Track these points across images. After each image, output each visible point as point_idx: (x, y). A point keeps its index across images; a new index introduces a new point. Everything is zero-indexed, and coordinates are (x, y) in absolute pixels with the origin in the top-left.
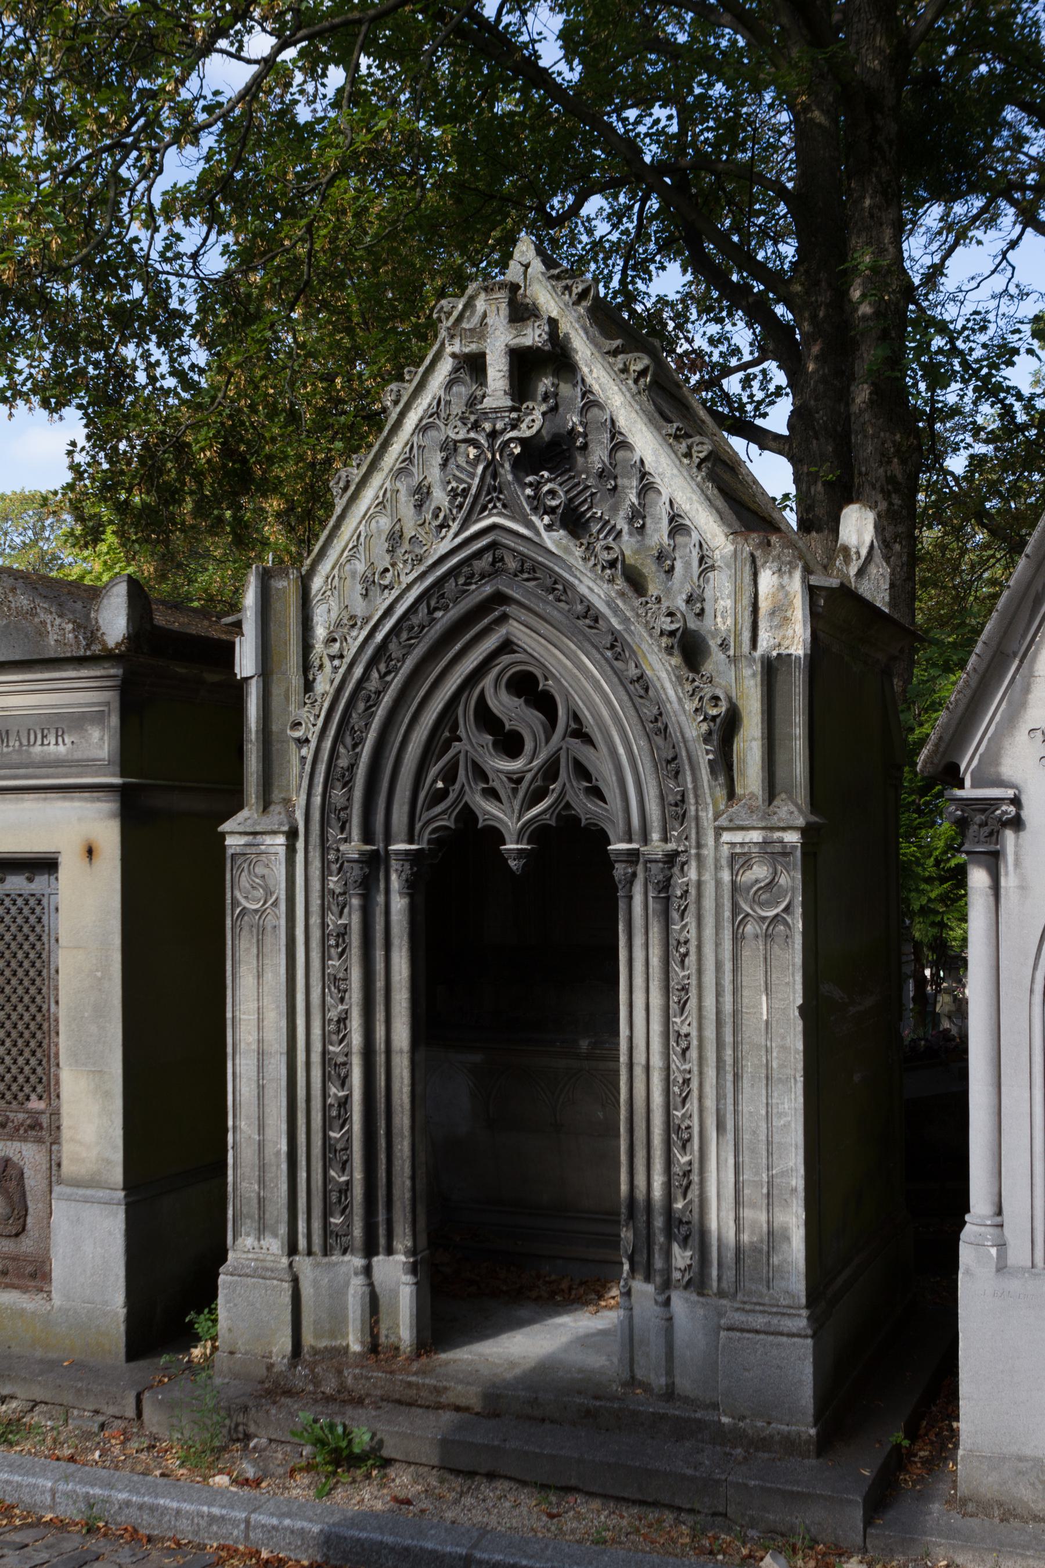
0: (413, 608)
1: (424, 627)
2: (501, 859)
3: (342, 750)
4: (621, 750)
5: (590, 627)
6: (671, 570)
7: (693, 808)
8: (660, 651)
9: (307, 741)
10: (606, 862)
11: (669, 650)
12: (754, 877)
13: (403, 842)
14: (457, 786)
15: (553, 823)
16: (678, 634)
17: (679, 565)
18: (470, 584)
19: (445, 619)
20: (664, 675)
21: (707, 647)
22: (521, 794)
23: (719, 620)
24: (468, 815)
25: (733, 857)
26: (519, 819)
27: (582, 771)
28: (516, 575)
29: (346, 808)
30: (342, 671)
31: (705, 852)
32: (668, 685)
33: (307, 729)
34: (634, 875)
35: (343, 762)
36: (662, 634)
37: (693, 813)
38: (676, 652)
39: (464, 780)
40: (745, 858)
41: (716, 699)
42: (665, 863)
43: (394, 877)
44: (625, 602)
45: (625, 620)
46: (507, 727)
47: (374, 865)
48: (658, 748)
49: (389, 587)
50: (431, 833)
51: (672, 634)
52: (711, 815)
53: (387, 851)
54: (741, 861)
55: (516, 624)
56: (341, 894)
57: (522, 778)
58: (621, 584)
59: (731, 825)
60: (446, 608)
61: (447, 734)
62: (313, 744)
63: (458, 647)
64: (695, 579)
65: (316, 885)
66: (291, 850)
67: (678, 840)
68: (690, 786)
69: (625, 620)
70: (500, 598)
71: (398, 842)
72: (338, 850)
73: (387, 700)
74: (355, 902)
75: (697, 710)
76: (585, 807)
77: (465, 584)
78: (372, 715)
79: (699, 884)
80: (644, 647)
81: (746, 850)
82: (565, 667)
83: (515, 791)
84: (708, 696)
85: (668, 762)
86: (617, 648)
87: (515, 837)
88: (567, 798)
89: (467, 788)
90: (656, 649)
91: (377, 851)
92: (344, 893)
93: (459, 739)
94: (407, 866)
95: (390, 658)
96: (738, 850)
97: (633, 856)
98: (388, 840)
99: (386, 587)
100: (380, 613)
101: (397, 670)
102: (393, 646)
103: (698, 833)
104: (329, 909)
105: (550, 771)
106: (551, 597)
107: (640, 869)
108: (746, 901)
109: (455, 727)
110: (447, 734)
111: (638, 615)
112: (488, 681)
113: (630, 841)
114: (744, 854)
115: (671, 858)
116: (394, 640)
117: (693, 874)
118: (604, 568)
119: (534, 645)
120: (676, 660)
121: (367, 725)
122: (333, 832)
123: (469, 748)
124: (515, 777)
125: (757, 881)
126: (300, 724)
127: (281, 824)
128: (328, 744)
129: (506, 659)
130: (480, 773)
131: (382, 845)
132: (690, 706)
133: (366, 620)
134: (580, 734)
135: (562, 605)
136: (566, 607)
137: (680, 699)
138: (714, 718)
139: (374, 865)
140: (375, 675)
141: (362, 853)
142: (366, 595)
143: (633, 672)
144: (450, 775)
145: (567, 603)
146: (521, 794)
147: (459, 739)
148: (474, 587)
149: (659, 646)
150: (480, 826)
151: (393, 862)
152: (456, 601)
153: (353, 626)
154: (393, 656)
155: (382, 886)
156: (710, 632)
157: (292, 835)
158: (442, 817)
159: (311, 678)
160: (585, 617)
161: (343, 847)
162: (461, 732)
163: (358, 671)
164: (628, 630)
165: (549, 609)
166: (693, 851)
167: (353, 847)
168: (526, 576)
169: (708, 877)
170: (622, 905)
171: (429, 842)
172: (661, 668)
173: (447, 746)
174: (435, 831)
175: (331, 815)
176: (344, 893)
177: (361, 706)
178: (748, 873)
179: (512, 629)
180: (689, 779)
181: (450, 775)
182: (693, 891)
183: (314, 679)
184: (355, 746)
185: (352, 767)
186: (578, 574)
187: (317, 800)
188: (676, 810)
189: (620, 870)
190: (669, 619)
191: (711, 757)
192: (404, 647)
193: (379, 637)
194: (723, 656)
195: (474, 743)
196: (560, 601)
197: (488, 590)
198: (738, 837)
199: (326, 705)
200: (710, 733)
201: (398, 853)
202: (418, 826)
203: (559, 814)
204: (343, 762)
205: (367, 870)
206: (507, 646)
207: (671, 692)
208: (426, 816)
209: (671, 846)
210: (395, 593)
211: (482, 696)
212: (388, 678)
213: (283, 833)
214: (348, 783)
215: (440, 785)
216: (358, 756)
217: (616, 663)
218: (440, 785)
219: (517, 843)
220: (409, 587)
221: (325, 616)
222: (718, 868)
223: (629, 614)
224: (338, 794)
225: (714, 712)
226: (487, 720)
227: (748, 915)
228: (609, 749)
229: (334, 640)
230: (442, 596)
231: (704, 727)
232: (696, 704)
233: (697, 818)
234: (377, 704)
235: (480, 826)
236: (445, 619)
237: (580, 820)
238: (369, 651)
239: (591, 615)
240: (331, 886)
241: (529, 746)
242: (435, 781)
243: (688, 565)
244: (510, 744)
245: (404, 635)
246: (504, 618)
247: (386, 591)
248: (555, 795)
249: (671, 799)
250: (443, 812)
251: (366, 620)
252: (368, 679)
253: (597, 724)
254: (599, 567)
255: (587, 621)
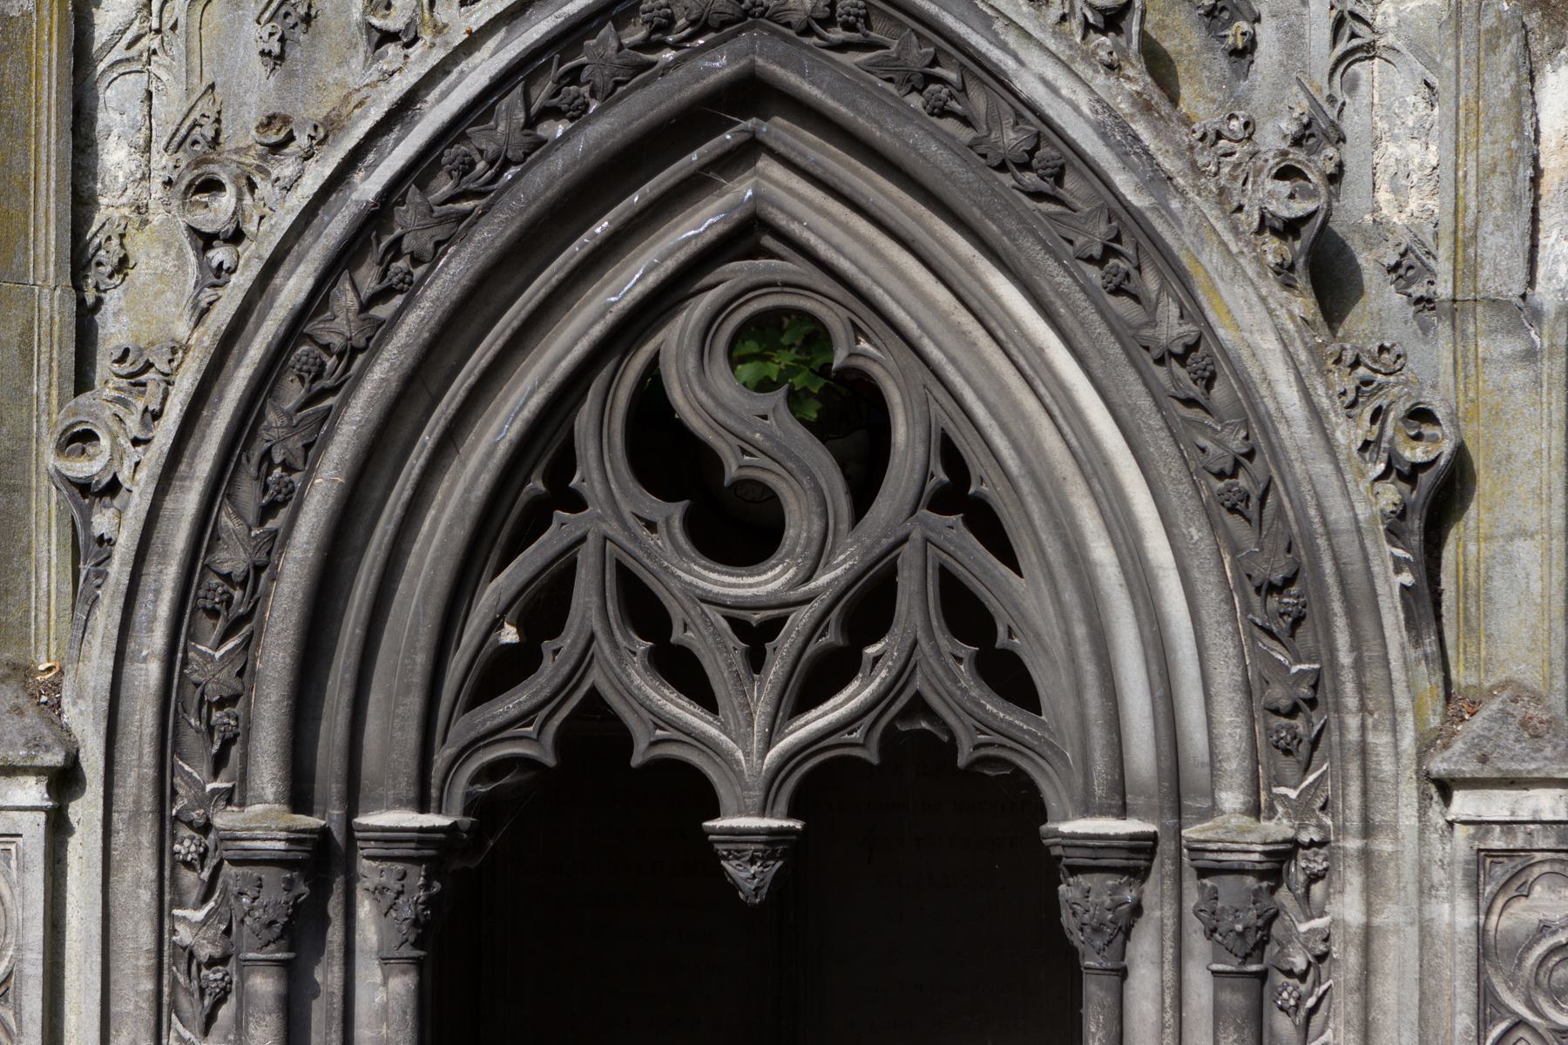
0: (479, 108)
1: (507, 164)
2: (704, 857)
3: (228, 521)
4: (1102, 552)
5: (1038, 196)
6: (1244, 53)
7: (1353, 722)
8: (1262, 275)
9: (113, 487)
10: (1045, 867)
11: (1284, 272)
12: (1534, 918)
13: (399, 803)
14: (569, 640)
15: (871, 755)
16: (1309, 232)
17: (1266, 33)
18: (661, 46)
19: (574, 146)
20: (1269, 344)
21: (1356, 270)
22: (776, 668)
23: (1383, 196)
24: (595, 729)
25: (1483, 858)
26: (769, 745)
27: (965, 612)
28: (807, 31)
29: (232, 700)
30: (241, 282)
31: (1383, 845)
32: (1280, 374)
33: (117, 454)
34: (1137, 910)
35: (232, 559)
36: (1265, 224)
37: (1353, 736)
38: (1302, 280)
39: (918, 618)
40: (1510, 865)
41: (1421, 415)
42: (1261, 875)
43: (365, 909)
44: (1158, 134)
45: (1158, 181)
46: (732, 471)
47: (321, 864)
48: (1235, 550)
49: (407, 38)
50: (476, 779)
51: (1290, 229)
52: (1408, 742)
53: (350, 829)
54: (1500, 872)
55: (777, 171)
56: (212, 963)
57: (779, 623)
58: (1137, 79)
59: (1487, 772)
60: (578, 114)
61: (537, 485)
62: (138, 500)
63: (601, 227)
64: (1321, 78)
65: (137, 934)
66: (58, 827)
67: (1300, 810)
68: (1345, 658)
69: (1158, 181)
70: (751, 93)
71: (379, 805)
72: (206, 828)
73: (382, 373)
74: (264, 985)
75: (1366, 445)
76: (969, 709)
77: (649, 45)
78: (328, 419)
79: (1368, 934)
80: (1211, 259)
81: (1519, 843)
82: (930, 303)
83: (756, 661)
84: (1401, 408)
85: (1273, 589)
86: (1125, 255)
87: (757, 795)
88: (918, 683)
89: (602, 642)
90: (1251, 270)
91: (325, 832)
92: (223, 960)
93: (576, 503)
94: (417, 876)
95: (395, 249)
96: (1496, 841)
97: (1136, 858)
98: (352, 803)
99: (388, 37)
100: (376, 114)
101: (410, 289)
102: (406, 216)
103: (1365, 792)
104: (174, 1007)
105: (869, 606)
106: (915, 101)
107: (1155, 892)
108: (1512, 981)
109: (566, 462)
110: (537, 485)
111: (1196, 170)
112: (675, 336)
113: (1123, 812)
114: (1510, 853)
115: (1281, 857)
116: (413, 194)
117: (1349, 908)
118: (1087, 26)
119: (839, 236)
120: (1303, 304)
121: (312, 449)
122: (193, 771)
123: (612, 528)
124: (756, 617)
125: (1544, 929)
126: (89, 436)
127: (36, 744)
128: (187, 502)
129: (737, 273)
130: (642, 608)
131: (336, 812)
132: (1349, 433)
133: (327, 131)
134: (956, 492)
135: (949, 124)
136: (966, 135)
137: (1316, 415)
138: (1411, 474)
139: (321, 864)
140: (346, 298)
141: (296, 839)
142: (281, 57)
143: (1171, 328)
144: (544, 608)
145: (966, 121)
146: (776, 668)
147: (576, 503)
148: (669, 55)
149: (1259, 260)
150: (637, 760)
151: (364, 865)
152: (610, 95)
153: (276, 148)
154: (408, 244)
155: (335, 935)
156: (1358, 228)
157: (65, 781)
158: (519, 726)
159: (90, 298)
160: (1025, 166)
161: (224, 819)
162: (586, 478)
163: (294, 287)
164: (1162, 207)
165: (915, 135)
166: (1353, 844)
167: (263, 819)
168: (837, 34)
169: (1389, 915)
170: (1095, 993)
171: (472, 805)
172: (1257, 320)
173: (534, 523)
174: (492, 771)
175: (194, 718)
176: (223, 960)
177: (293, 392)
178: (1518, 906)
179: (767, 187)
180: (1342, 639)
181: (544, 608)
182: (1348, 958)
183: (99, 302)
184: (268, 511)
185: (260, 571)
186: (1011, 39)
187: (147, 673)
188: (1295, 725)
189: (1082, 898)
190: (1285, 187)
191: (1407, 578)
192: (443, 220)
193: (368, 186)
194: (1398, 299)
195: (617, 514)
196: (944, 113)
197: (720, 66)
198: (1497, 805)
199: (186, 383)
200: (1402, 514)
201: (390, 837)
202: (441, 757)
203: (890, 727)
204: (232, 559)
205: (303, 889)
206: (748, 235)
207: (1289, 394)
208: (466, 726)
209: (1279, 828)
210: (422, 59)
211: (652, 376)
212: (382, 311)
213: (38, 771)
214: (243, 624)
215: (510, 635)
216: (276, 542)
217: (1112, 301)
218: (510, 635)
219: (762, 813)
220: (474, 40)
221: (137, 111)
222: (1425, 891)
223: (1169, 164)
224: (211, 653)
225: (1416, 453)
226: (665, 451)
227: (1520, 1023)
228: (1067, 546)
229: (212, 186)
230: (574, 76)
231: (1390, 494)
232: (1363, 429)
233: (1364, 750)
234: (345, 386)
235: (637, 760)
236: (580, 145)
237: (952, 747)
238: (335, 227)
239: (1045, 161)
240: (184, 935)
241: (799, 527)
242: (496, 625)
243: (1294, 38)
244: (738, 526)
245: (443, 186)
246: (752, 149)
247: (392, 49)
248: (883, 674)
249: (1279, 694)
250: (524, 718)
251: (327, 131)
252: (325, 305)
253: (1032, 474)
254: (1075, 25)
255: (1029, 178)
